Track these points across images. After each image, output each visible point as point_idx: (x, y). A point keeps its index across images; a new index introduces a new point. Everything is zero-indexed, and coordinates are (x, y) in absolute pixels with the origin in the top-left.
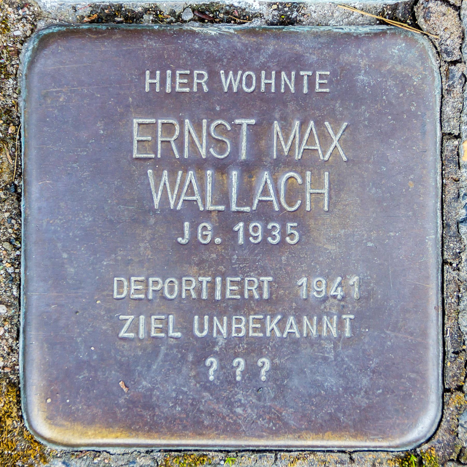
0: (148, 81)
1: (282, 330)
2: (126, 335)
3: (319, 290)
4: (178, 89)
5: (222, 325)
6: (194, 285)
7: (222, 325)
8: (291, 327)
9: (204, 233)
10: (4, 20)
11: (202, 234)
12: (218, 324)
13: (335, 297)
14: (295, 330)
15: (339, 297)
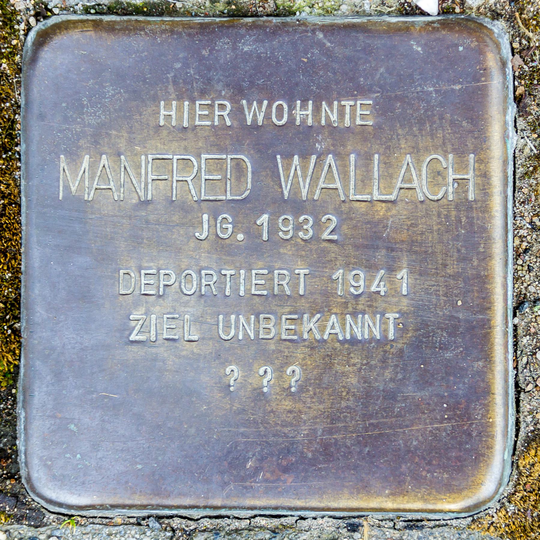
0: (163, 112)
1: (322, 329)
2: (138, 338)
3: (356, 285)
4: (197, 123)
5: (332, 111)
6: (215, 279)
7: (332, 111)
8: (333, 327)
9: (224, 226)
10: (535, 16)
11: (221, 226)
12: (327, 109)
13: (378, 292)
14: (337, 330)
15: (382, 293)
